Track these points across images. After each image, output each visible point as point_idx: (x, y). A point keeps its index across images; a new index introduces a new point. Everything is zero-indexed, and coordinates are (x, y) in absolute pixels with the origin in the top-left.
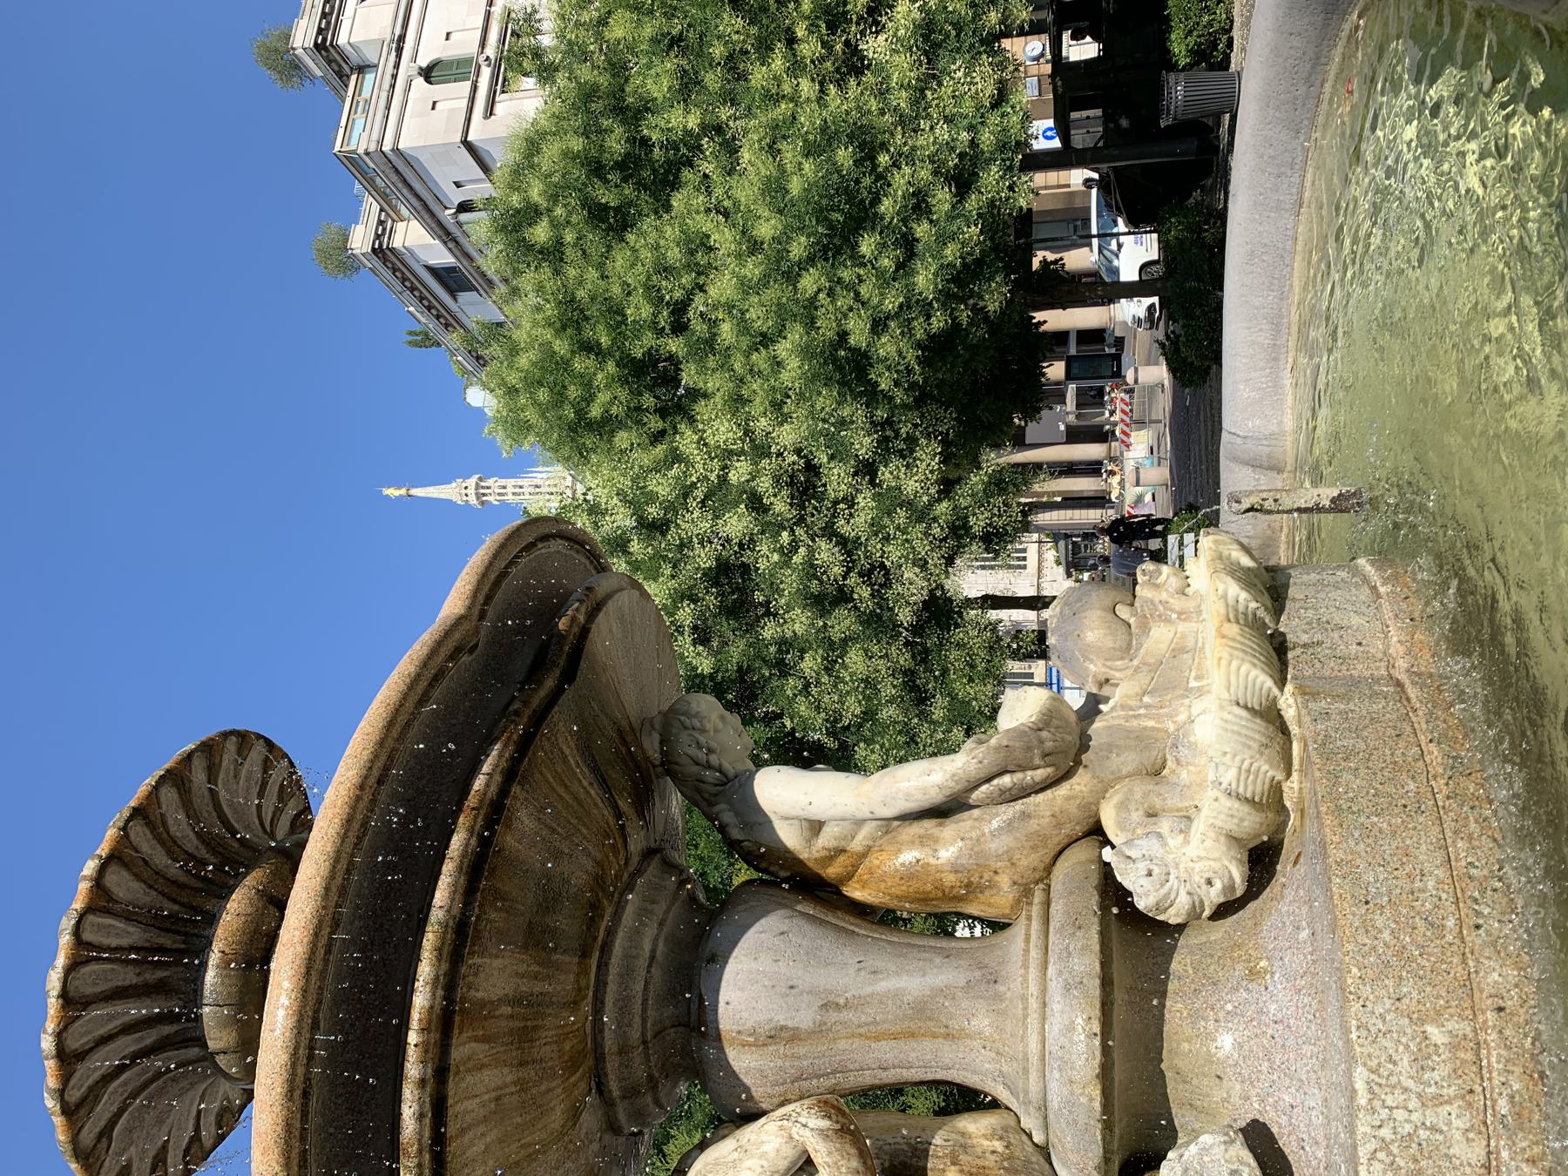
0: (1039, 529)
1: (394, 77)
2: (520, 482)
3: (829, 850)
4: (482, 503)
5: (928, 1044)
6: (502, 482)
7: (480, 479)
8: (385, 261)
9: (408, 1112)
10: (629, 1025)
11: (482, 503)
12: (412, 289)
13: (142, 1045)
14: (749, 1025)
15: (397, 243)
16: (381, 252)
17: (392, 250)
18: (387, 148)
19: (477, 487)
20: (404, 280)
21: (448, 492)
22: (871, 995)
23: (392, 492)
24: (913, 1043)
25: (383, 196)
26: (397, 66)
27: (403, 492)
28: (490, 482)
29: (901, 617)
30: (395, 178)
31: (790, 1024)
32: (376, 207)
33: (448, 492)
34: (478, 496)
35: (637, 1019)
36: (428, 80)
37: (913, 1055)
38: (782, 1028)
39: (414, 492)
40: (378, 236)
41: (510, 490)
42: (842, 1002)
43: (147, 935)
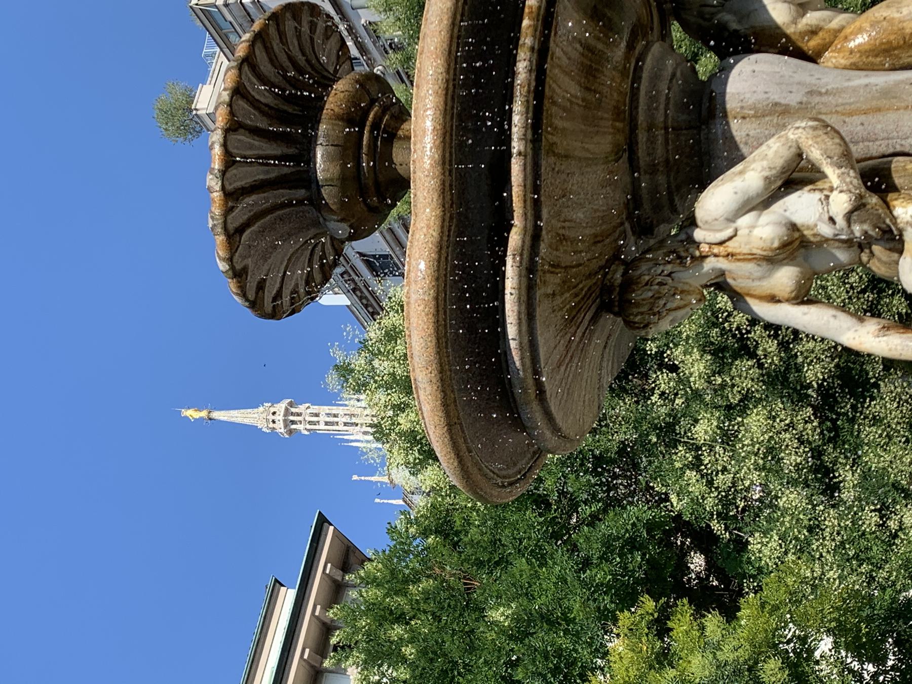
2: (335, 410)
3: (811, 26)
4: (290, 432)
5: (892, 116)
6: (315, 409)
7: (291, 405)
9: (522, 67)
10: (657, 109)
11: (290, 432)
13: (268, 177)
14: (750, 102)
19: (287, 412)
21: (252, 417)
22: (847, 88)
23: (191, 414)
24: (879, 116)
27: (204, 414)
28: (301, 408)
29: (810, 374)
31: (783, 102)
33: (252, 417)
34: (287, 423)
35: (662, 107)
37: (879, 126)
38: (776, 104)
39: (216, 415)
41: (323, 418)
42: (823, 90)
43: (276, 102)
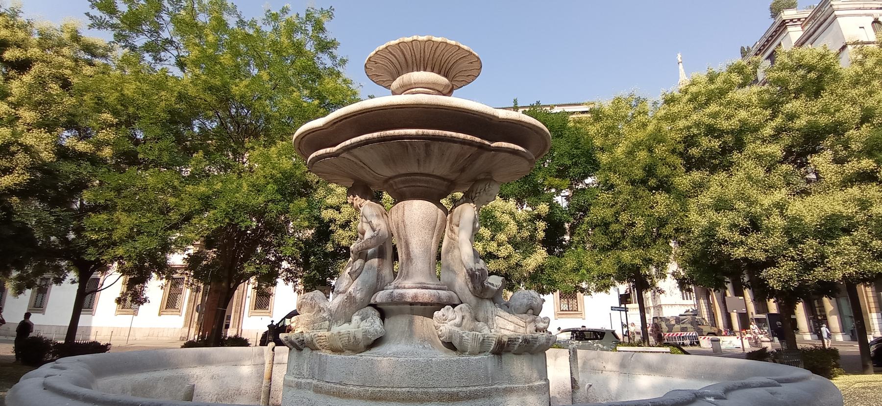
0: (698, 303)
1: (871, 9)
8: (780, 26)
12: (768, 41)
15: (789, 29)
16: (783, 25)
17: (786, 28)
18: (836, 13)
20: (772, 36)
23: (679, 56)
25: (813, 17)
26: (877, 9)
30: (822, 20)
32: (806, 16)
36: (873, 22)
40: (791, 20)
